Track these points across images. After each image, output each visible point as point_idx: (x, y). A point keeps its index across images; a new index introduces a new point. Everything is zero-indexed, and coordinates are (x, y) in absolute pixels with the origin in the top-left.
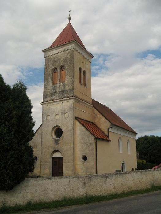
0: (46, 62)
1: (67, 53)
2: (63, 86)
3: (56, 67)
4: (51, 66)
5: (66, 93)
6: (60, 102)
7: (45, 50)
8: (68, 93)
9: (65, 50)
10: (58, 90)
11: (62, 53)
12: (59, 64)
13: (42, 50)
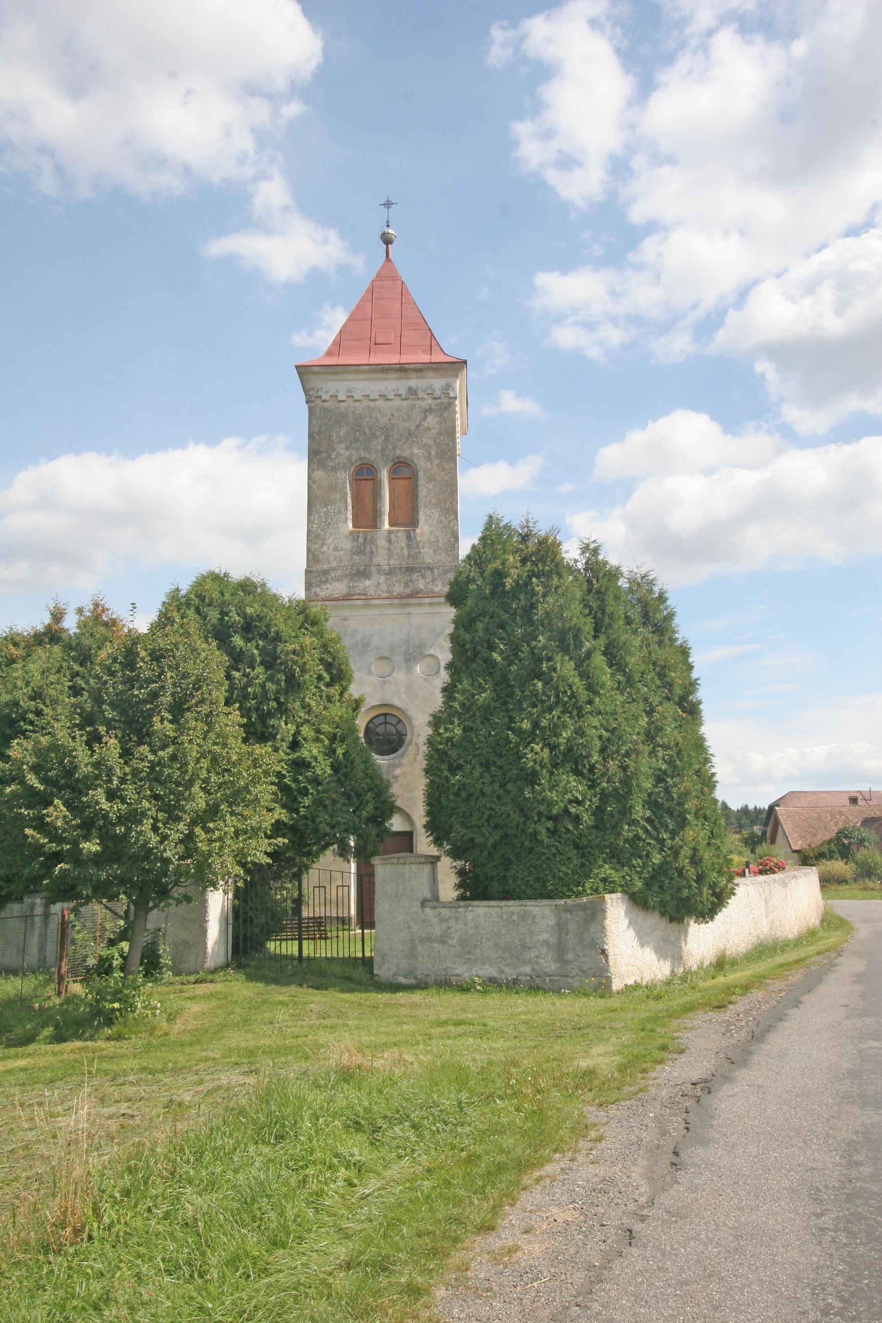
0: (314, 422)
1: (425, 411)
2: (408, 546)
3: (372, 457)
4: (342, 445)
5: (423, 576)
6: (399, 611)
7: (363, 367)
8: (434, 580)
9: (412, 392)
10: (381, 559)
11: (397, 402)
12: (384, 450)
13: (297, 367)
